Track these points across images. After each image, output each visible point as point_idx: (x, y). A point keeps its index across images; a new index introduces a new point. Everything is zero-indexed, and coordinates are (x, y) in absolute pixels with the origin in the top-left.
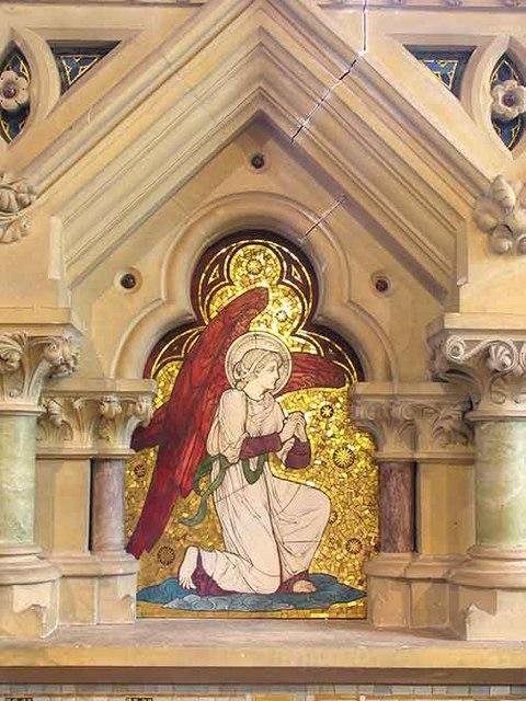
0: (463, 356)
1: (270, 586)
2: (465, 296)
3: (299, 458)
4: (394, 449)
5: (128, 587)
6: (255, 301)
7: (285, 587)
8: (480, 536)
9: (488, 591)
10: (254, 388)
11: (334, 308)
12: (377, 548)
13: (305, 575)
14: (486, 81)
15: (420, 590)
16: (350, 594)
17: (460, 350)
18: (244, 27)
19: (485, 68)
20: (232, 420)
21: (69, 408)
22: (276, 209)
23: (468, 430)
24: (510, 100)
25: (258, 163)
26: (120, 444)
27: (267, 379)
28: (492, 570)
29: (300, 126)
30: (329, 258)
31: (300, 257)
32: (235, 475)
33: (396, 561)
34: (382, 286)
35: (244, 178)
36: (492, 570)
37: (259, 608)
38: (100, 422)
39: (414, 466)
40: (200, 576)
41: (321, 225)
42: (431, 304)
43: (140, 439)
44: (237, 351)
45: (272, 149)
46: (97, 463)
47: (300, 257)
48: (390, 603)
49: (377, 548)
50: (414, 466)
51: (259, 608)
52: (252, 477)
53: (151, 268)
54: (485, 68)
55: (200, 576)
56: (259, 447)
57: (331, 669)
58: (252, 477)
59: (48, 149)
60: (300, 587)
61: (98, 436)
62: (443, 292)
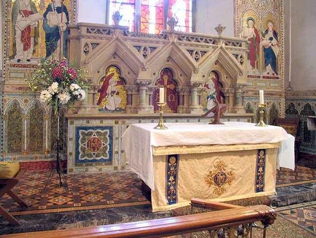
0: (139, 82)
1: (114, 109)
2: (139, 76)
3: (118, 94)
4: (130, 93)
5: (98, 109)
6: (113, 74)
7: (116, 110)
8: (140, 102)
9: (140, 108)
10: (112, 85)
11: (123, 76)
12: (127, 104)
13: (118, 108)
14: (194, 54)
15: (132, 109)
16: (123, 110)
17: (138, 82)
18: (171, 47)
19: (194, 52)
20: (110, 89)
21: (91, 88)
22: (117, 64)
23: (138, 91)
24: (145, 53)
25: (114, 58)
26: (96, 92)
27: (113, 84)
28: (140, 106)
29: (121, 55)
30: (122, 69)
31: (118, 69)
32: (110, 96)
33: (129, 106)
34: (129, 73)
35: (113, 60)
36: (140, 106)
37: (113, 111)
38: (95, 89)
39: (132, 95)
40: (105, 108)
41: (123, 67)
42: (135, 76)
43: (98, 91)
44: (110, 81)
45: (116, 56)
46: (94, 94)
47: (118, 69)
48: (129, 110)
49: (127, 104)
50: (132, 95)
51: (113, 111)
52: (112, 96)
53: (101, 70)
54: (194, 52)
55: (105, 108)
56: (113, 92)
57: (295, 151)
58: (112, 96)
59: (223, 68)
60: (118, 109)
61: (94, 91)
62: (136, 74)
